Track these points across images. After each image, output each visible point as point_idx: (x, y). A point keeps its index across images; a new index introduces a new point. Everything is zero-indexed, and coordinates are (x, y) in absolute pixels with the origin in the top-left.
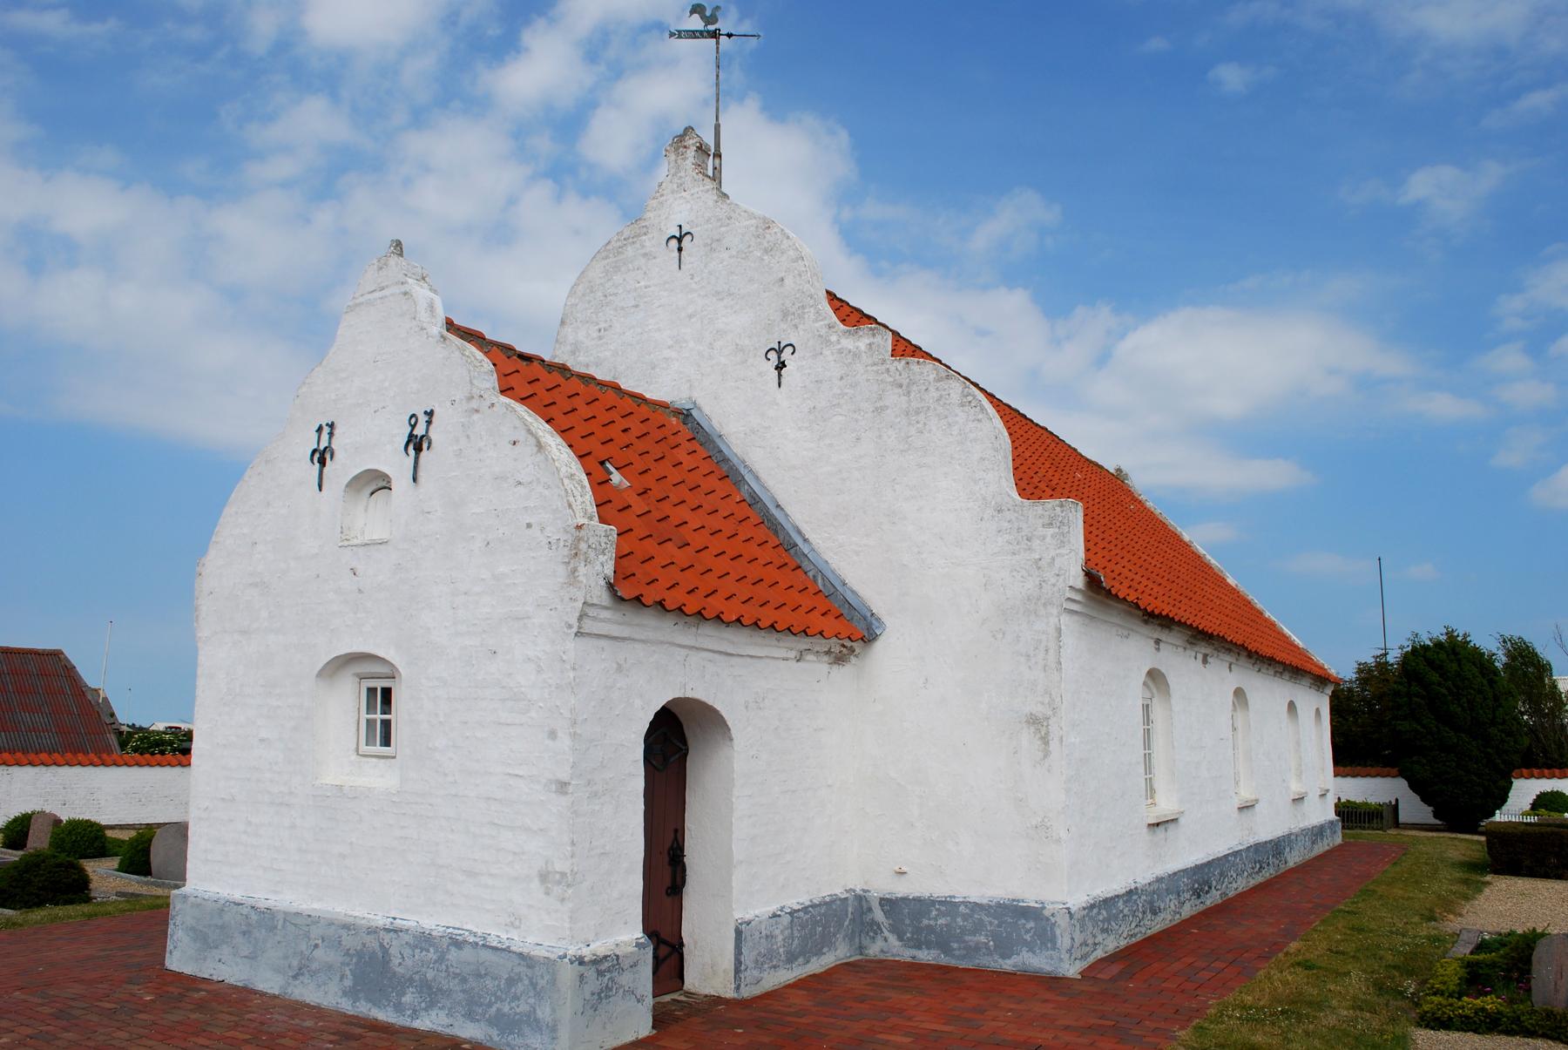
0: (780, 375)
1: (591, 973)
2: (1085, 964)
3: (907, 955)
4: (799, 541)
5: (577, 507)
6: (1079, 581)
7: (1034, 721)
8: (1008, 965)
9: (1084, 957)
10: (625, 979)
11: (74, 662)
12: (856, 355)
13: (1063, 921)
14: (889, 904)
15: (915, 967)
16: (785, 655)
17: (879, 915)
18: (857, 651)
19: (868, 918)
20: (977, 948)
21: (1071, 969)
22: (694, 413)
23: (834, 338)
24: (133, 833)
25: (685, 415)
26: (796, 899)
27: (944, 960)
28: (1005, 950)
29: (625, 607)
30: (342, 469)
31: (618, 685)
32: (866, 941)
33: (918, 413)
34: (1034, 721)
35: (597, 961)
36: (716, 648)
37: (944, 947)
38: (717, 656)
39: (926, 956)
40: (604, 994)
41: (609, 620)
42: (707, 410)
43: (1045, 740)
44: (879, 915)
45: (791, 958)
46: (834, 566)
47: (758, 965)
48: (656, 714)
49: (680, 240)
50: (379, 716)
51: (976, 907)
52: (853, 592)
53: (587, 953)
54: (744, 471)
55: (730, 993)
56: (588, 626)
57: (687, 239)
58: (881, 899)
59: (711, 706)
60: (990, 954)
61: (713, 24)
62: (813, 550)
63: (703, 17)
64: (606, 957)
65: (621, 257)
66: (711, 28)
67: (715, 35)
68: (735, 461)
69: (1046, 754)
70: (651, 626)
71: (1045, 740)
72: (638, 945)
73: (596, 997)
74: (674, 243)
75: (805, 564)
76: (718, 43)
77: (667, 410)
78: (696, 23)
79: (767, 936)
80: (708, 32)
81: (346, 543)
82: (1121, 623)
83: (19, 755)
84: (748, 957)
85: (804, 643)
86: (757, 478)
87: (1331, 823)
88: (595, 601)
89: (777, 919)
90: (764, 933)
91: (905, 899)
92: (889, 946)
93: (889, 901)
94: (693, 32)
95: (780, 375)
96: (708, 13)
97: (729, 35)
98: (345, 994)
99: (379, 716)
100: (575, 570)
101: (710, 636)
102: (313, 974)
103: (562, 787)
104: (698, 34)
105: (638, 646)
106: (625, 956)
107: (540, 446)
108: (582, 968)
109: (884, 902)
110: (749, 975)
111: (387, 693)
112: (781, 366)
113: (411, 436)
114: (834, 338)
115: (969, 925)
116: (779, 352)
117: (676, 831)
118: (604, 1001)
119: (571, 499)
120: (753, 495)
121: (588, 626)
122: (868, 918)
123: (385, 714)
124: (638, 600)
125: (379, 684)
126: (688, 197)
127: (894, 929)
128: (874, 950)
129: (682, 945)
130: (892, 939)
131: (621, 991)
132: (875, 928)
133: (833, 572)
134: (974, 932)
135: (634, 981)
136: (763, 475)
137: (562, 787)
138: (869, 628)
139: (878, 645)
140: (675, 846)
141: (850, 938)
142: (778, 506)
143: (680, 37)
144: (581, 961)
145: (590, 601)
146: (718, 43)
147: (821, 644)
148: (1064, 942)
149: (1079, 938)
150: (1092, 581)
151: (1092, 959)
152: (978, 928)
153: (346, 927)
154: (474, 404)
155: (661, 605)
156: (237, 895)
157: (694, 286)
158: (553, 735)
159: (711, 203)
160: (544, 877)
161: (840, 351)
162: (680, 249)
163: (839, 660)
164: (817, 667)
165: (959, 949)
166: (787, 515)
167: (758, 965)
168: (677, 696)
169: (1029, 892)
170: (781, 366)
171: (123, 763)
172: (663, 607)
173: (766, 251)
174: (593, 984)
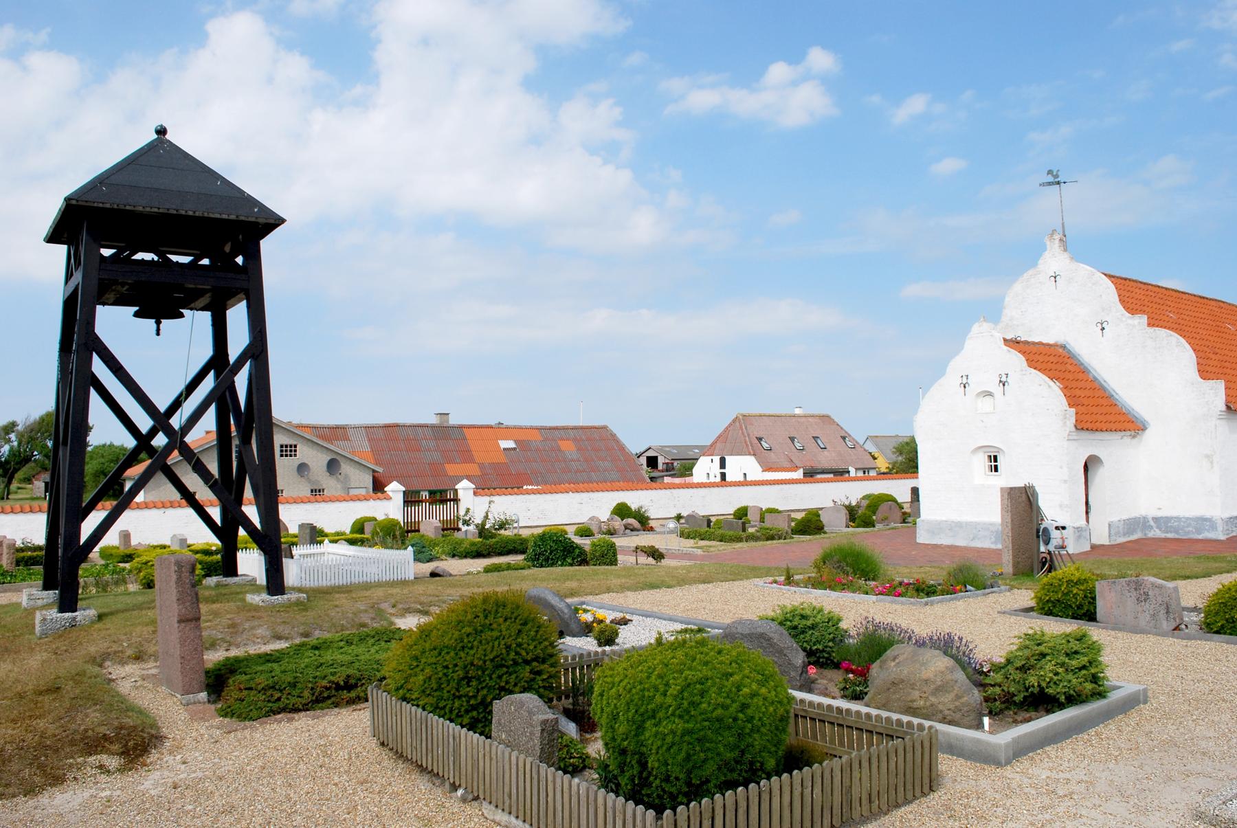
2: (1228, 537)
3: (1163, 535)
6: (1224, 408)
7: (1207, 456)
8: (1200, 537)
9: (1228, 534)
10: (1084, 533)
11: (615, 431)
12: (1134, 326)
13: (1219, 522)
14: (1156, 519)
15: (1166, 540)
17: (1152, 523)
19: (1148, 524)
20: (1189, 532)
21: (1222, 537)
22: (1067, 346)
23: (1124, 319)
24: (803, 515)
25: (1064, 347)
26: (1125, 517)
27: (1177, 536)
28: (1199, 531)
30: (974, 388)
32: (1147, 532)
33: (1159, 348)
34: (1207, 456)
37: (1176, 532)
39: (1170, 535)
40: (1079, 537)
41: (1075, 435)
42: (1072, 344)
43: (1212, 463)
44: (1152, 523)
45: (1124, 535)
47: (1115, 535)
50: (993, 464)
51: (1188, 519)
55: (1107, 542)
60: (1193, 533)
63: (1053, 176)
66: (1056, 180)
67: (1058, 183)
68: (1086, 365)
69: (1212, 467)
70: (1086, 435)
71: (1212, 463)
74: (1053, 278)
75: (1117, 403)
78: (1050, 179)
83: (516, 490)
84: (1112, 532)
85: (1123, 433)
86: (1096, 371)
91: (1161, 517)
92: (1156, 533)
93: (1156, 518)
98: (992, 543)
99: (993, 464)
100: (1065, 422)
101: (1099, 435)
102: (979, 539)
103: (1065, 481)
107: (1049, 386)
109: (1153, 518)
110: (1112, 538)
111: (995, 457)
112: (1103, 329)
113: (1000, 381)
114: (1124, 319)
115: (1185, 525)
116: (1102, 324)
120: (1094, 377)
122: (1148, 524)
124: (1082, 429)
125: (992, 455)
128: (1151, 534)
130: (1157, 531)
132: (1151, 527)
134: (1187, 527)
136: (1098, 371)
137: (1065, 481)
138: (1144, 425)
139: (1147, 431)
141: (1142, 531)
147: (1128, 433)
148: (1220, 529)
149: (1226, 528)
150: (1228, 408)
151: (1231, 535)
152: (1189, 525)
153: (991, 524)
154: (1024, 372)
155: (1087, 429)
156: (944, 519)
158: (1061, 467)
160: (1061, 506)
161: (1127, 324)
163: (1134, 437)
164: (1127, 440)
167: (1115, 535)
169: (1208, 514)
170: (1103, 329)
173: (1094, 284)
174: (1077, 534)
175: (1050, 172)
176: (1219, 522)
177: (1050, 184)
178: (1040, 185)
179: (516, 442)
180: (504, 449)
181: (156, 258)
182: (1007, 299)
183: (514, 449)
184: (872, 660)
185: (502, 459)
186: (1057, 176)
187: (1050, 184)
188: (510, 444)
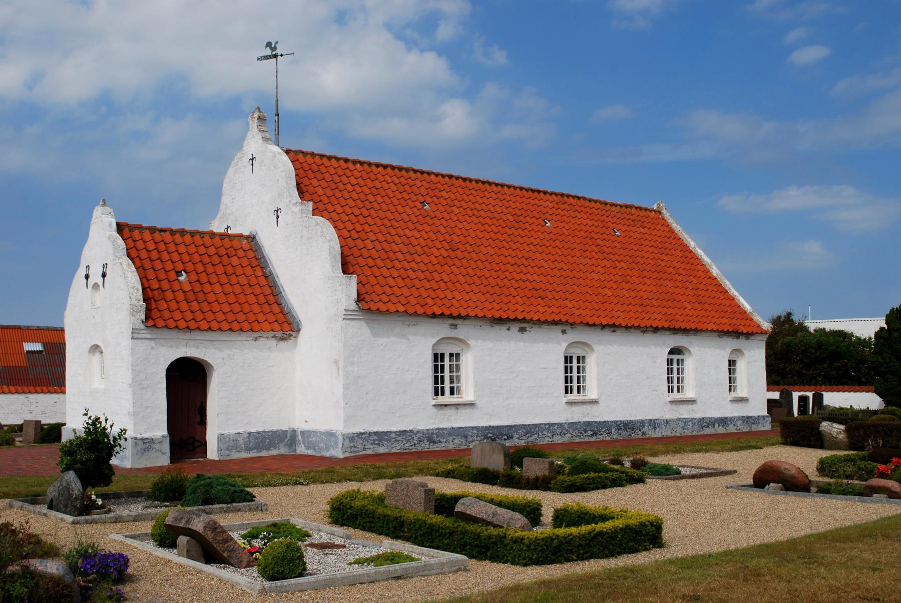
0: (104, 280)
1: (140, 443)
4: (282, 291)
5: (133, 298)
8: (327, 454)
10: (157, 446)
15: (738, 433)
16: (246, 339)
18: (294, 335)
29: (151, 329)
31: (152, 354)
35: (142, 439)
36: (203, 338)
38: (205, 342)
45: (249, 449)
46: (291, 301)
48: (172, 363)
49: (252, 160)
52: (295, 311)
53: (139, 436)
54: (269, 262)
55: (216, 459)
56: (136, 336)
57: (255, 159)
58: (301, 431)
59: (203, 359)
61: (275, 51)
62: (286, 294)
64: (147, 438)
65: (238, 167)
66: (274, 53)
67: (275, 56)
68: (266, 257)
72: (163, 436)
73: (143, 450)
76: (277, 60)
77: (242, 238)
78: (268, 52)
79: (233, 440)
80: (273, 55)
81: (94, 307)
82: (149, 336)
86: (272, 265)
87: (764, 417)
88: (137, 328)
89: (240, 435)
90: (231, 439)
94: (267, 56)
95: (104, 280)
96: (273, 46)
97: (282, 55)
104: (268, 57)
105: (162, 341)
106: (156, 439)
108: (136, 441)
109: (302, 433)
112: (278, 217)
116: (277, 211)
117: (202, 403)
118: (147, 452)
119: (131, 295)
121: (136, 336)
123: (454, 381)
126: (255, 141)
127: (304, 444)
129: (206, 443)
131: (155, 450)
133: (291, 304)
135: (161, 447)
139: (301, 332)
140: (202, 408)
142: (277, 276)
143: (261, 60)
144: (136, 439)
145: (134, 327)
146: (277, 60)
157: (256, 181)
159: (261, 144)
162: (252, 165)
165: (318, 449)
166: (279, 280)
168: (182, 356)
171: (54, 391)
172: (167, 327)
175: (269, 45)
176: (340, 438)
177: (267, 57)
178: (258, 59)
179: (44, 345)
180: (28, 352)
181: (886, 328)
182: (225, 185)
183: (40, 352)
184: (808, 478)
185: (23, 362)
186: (274, 49)
187: (267, 57)
188: (38, 347)
